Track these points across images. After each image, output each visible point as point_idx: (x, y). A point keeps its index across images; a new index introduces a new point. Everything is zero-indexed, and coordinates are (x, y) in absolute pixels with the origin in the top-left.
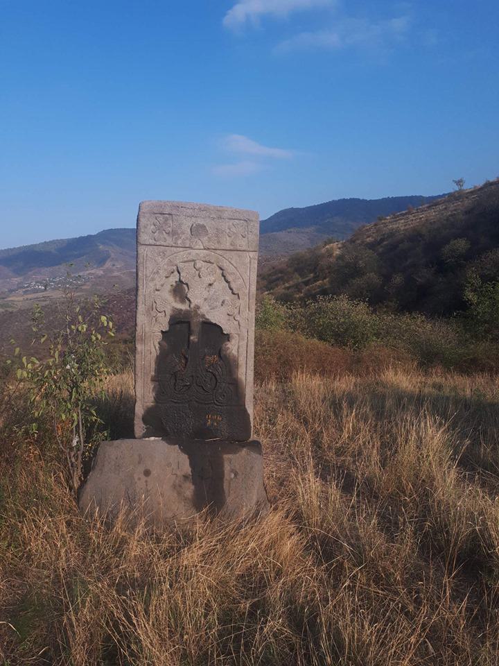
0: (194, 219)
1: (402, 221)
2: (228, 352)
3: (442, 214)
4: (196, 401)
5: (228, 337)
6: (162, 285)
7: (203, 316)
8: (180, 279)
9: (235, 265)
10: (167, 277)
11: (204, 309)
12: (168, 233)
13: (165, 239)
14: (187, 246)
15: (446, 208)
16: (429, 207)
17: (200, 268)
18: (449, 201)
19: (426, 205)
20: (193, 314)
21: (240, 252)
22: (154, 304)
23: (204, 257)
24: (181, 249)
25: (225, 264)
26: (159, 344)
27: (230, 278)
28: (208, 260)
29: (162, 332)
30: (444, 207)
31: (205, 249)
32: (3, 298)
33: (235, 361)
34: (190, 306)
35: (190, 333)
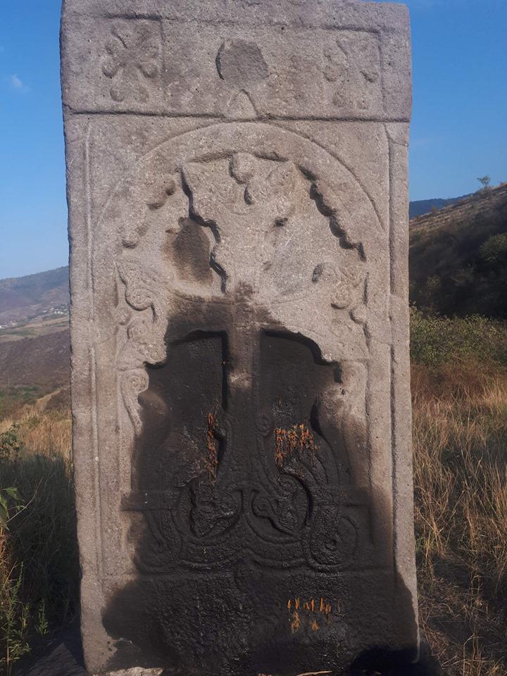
0: (224, 30)
1: (427, 223)
2: (340, 413)
3: (469, 214)
4: (256, 563)
5: (336, 372)
6: (142, 231)
7: (263, 314)
8: (191, 208)
9: (348, 161)
10: (154, 207)
11: (265, 295)
12: (151, 76)
13: (142, 91)
14: (209, 110)
15: (473, 207)
16: (453, 208)
17: (249, 176)
18: (476, 200)
19: (451, 206)
20: (233, 309)
21: (363, 125)
22: (121, 287)
23: (260, 143)
24: (192, 122)
25: (321, 162)
26: (140, 400)
27: (335, 200)
28: (269, 151)
29: (148, 366)
30: (470, 206)
31: (260, 119)
32: (23, 326)
33: (359, 439)
34: (223, 288)
35: (228, 362)
